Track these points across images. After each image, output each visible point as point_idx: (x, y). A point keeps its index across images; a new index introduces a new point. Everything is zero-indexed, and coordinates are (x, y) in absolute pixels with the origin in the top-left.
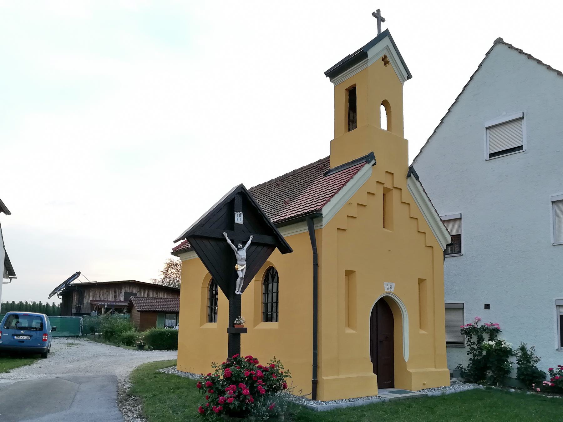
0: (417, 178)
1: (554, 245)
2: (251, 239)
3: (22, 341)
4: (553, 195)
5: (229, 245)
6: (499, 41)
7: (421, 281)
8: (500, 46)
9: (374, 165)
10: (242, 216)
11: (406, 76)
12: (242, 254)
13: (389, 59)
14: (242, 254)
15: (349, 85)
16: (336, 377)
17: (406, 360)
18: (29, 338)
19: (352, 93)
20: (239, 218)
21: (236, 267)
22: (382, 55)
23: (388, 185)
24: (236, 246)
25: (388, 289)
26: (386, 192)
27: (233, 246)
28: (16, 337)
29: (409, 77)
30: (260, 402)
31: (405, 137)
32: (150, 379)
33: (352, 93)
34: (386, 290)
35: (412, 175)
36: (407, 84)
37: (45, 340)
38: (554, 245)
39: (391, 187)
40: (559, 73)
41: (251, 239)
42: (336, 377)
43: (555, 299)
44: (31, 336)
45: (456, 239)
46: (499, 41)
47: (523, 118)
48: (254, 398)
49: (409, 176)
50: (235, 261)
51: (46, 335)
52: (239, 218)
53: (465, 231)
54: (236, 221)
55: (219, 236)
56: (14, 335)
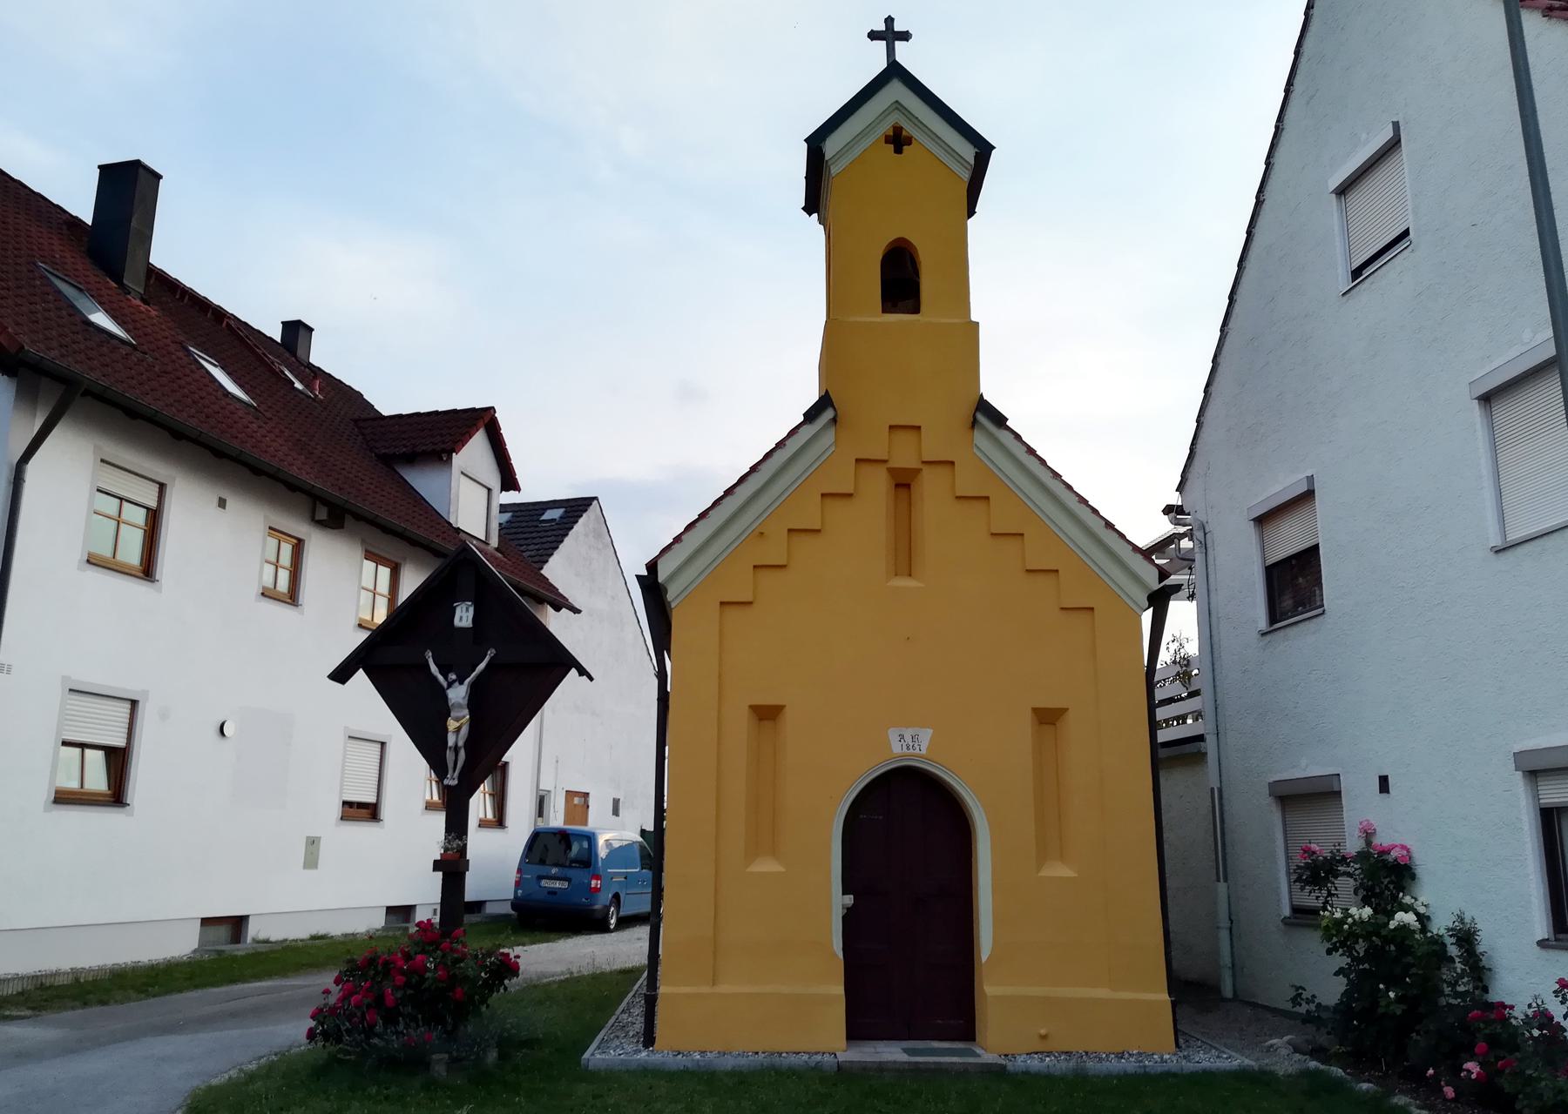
1: (1498, 551)
2: (487, 659)
3: (553, 892)
5: (435, 679)
9: (834, 420)
10: (471, 610)
12: (458, 694)
13: (909, 129)
14: (458, 694)
16: (705, 989)
18: (566, 885)
22: (886, 128)
23: (904, 459)
24: (446, 678)
26: (903, 482)
27: (441, 678)
28: (544, 883)
30: (1539, 1079)
31: (974, 318)
32: (1457, 995)
34: (897, 748)
35: (980, 417)
37: (597, 890)
38: (1498, 551)
39: (912, 463)
40: (1309, 7)
41: (487, 659)
42: (705, 989)
44: (568, 880)
45: (1306, 562)
47: (1394, 145)
49: (974, 423)
51: (597, 877)
53: (1328, 529)
54: (457, 622)
56: (540, 878)
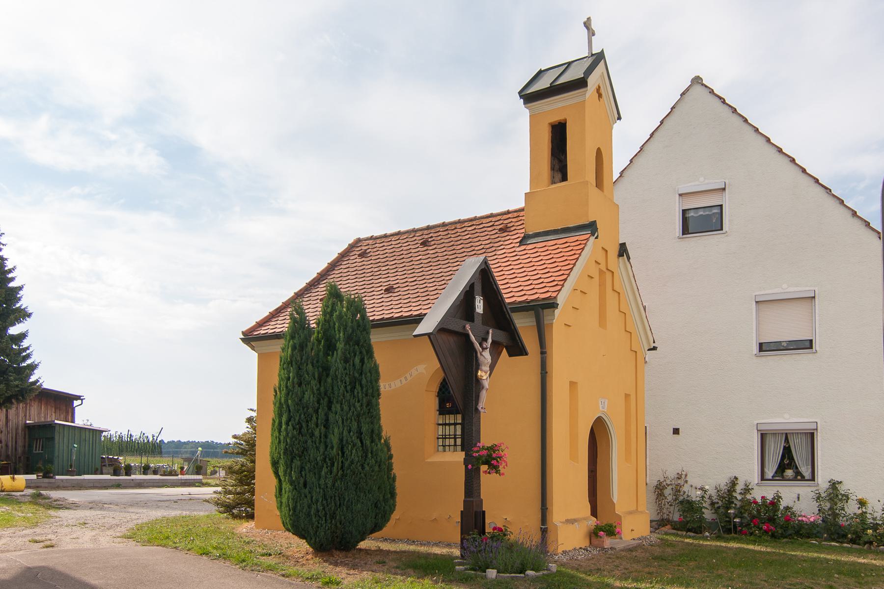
0: (629, 258)
4: (757, 293)
6: (697, 80)
7: (627, 396)
8: (698, 88)
9: (596, 238)
11: (616, 116)
13: (602, 91)
15: (556, 118)
17: (615, 501)
19: (559, 134)
20: (479, 306)
21: (479, 373)
25: (602, 408)
29: (619, 118)
33: (559, 134)
36: (617, 127)
43: (756, 422)
46: (697, 80)
47: (724, 189)
48: (93, 529)
50: (478, 366)
52: (479, 306)
55: (461, 330)
